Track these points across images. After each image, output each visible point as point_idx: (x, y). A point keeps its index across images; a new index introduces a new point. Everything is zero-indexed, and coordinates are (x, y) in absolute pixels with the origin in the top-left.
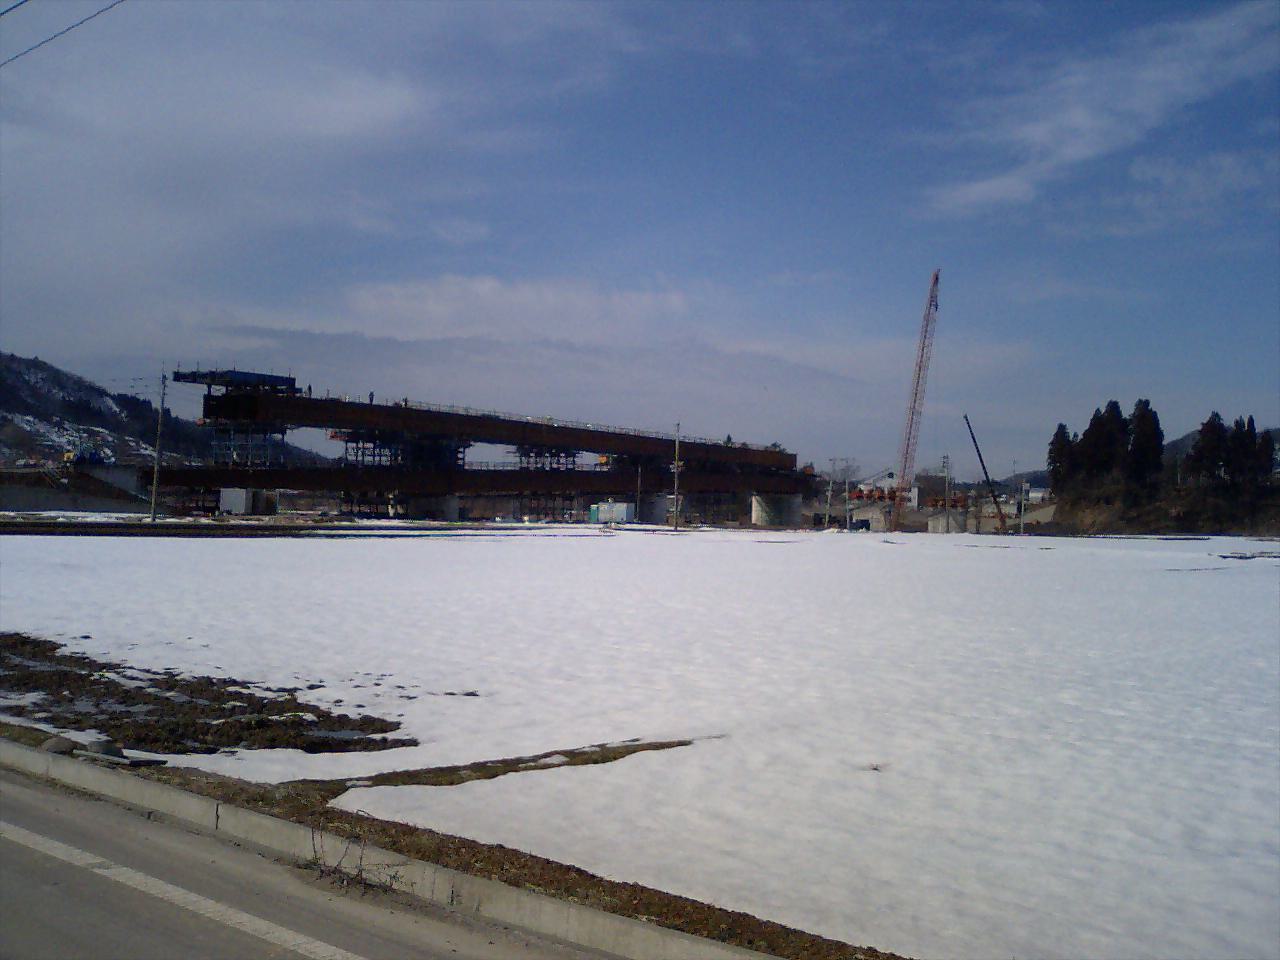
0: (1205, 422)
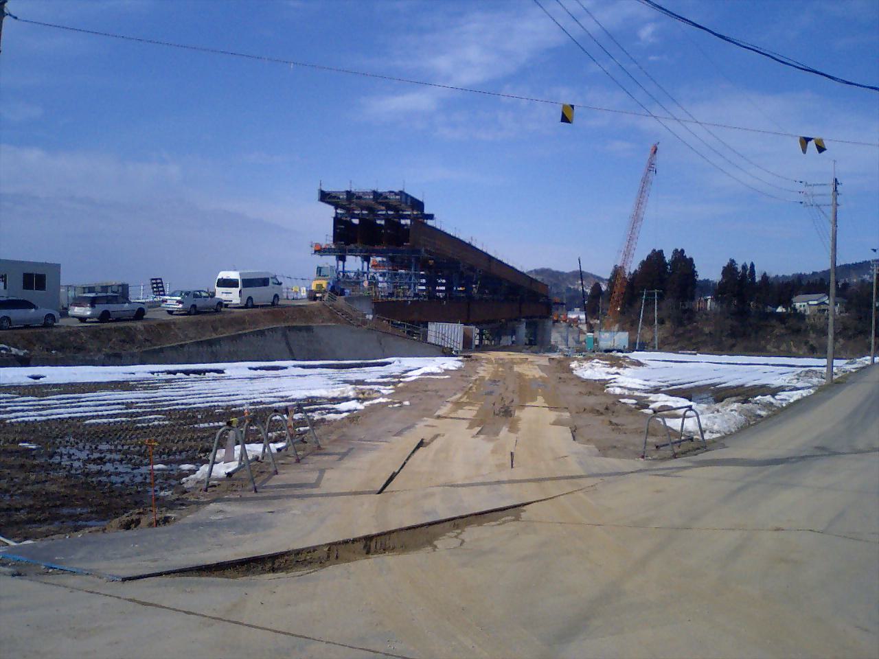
0: (725, 266)
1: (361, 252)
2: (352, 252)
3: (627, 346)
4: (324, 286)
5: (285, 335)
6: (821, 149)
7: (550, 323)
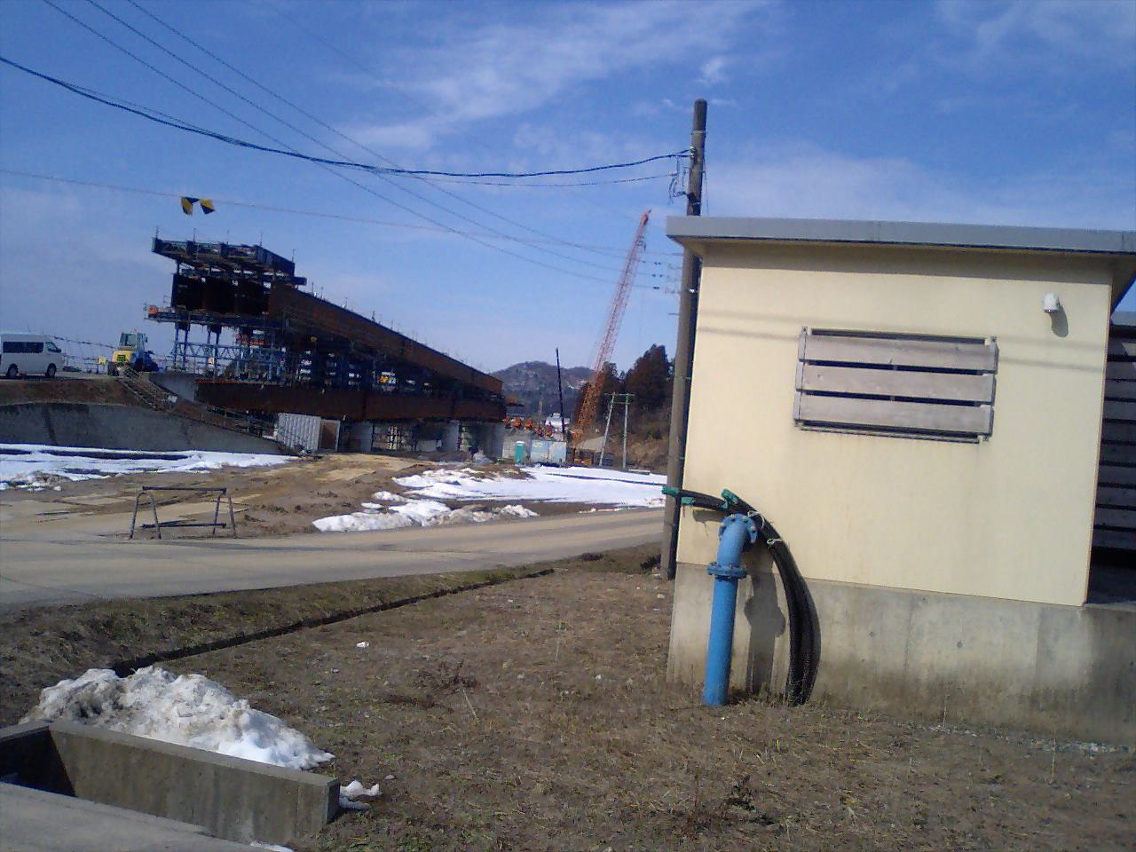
1: (208, 319)
2: (197, 320)
3: (564, 460)
4: (128, 358)
5: (46, 414)
6: (207, 210)
7: (503, 428)
